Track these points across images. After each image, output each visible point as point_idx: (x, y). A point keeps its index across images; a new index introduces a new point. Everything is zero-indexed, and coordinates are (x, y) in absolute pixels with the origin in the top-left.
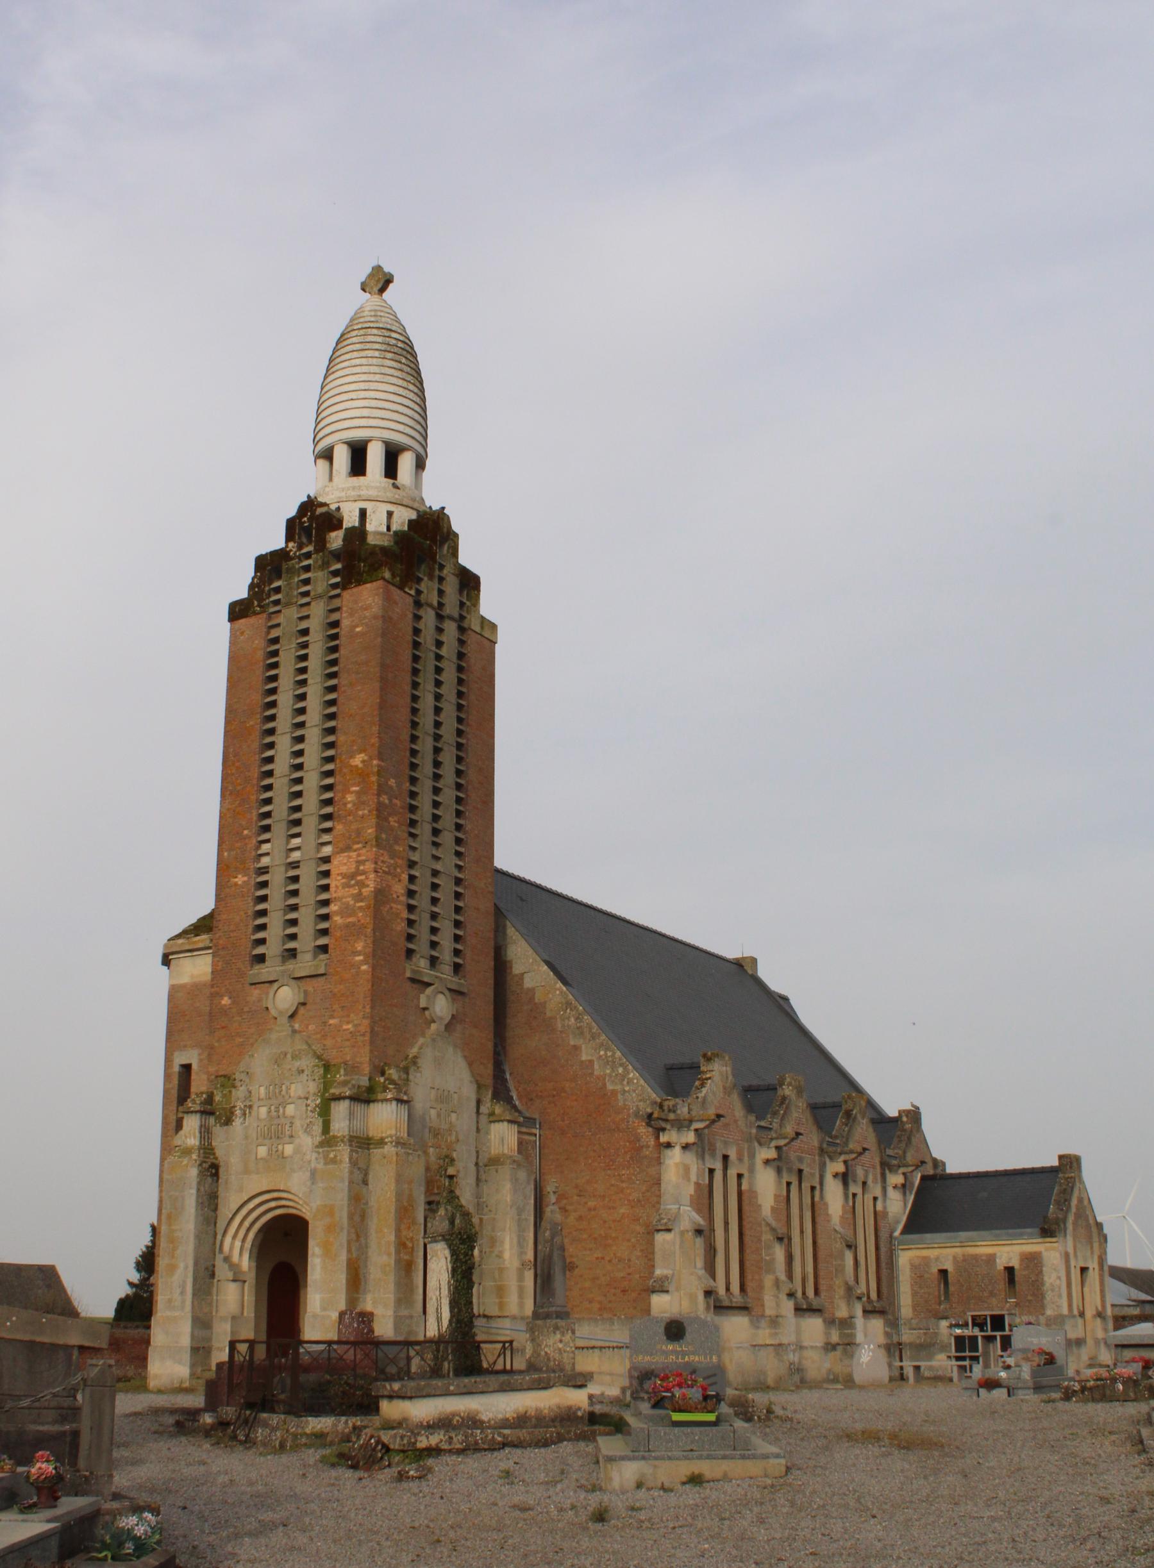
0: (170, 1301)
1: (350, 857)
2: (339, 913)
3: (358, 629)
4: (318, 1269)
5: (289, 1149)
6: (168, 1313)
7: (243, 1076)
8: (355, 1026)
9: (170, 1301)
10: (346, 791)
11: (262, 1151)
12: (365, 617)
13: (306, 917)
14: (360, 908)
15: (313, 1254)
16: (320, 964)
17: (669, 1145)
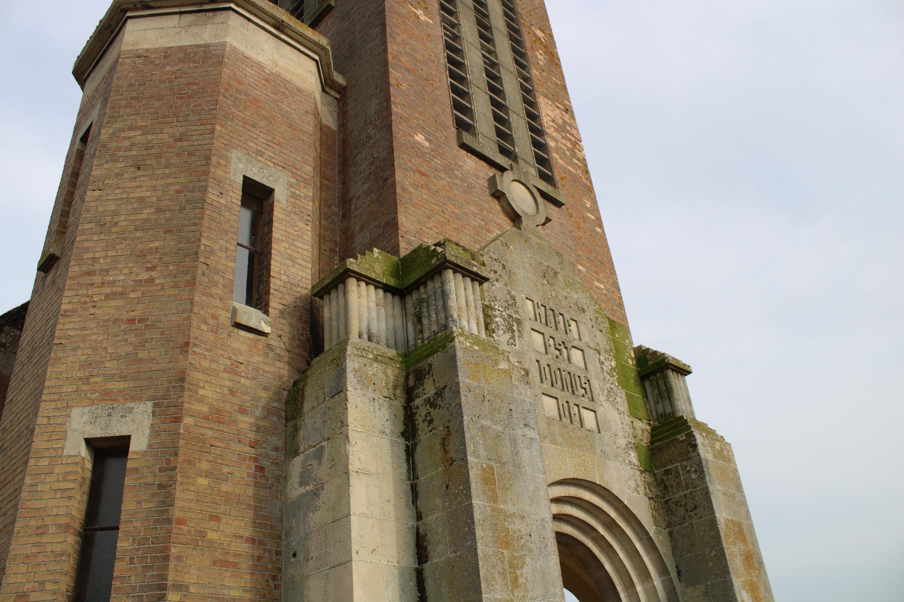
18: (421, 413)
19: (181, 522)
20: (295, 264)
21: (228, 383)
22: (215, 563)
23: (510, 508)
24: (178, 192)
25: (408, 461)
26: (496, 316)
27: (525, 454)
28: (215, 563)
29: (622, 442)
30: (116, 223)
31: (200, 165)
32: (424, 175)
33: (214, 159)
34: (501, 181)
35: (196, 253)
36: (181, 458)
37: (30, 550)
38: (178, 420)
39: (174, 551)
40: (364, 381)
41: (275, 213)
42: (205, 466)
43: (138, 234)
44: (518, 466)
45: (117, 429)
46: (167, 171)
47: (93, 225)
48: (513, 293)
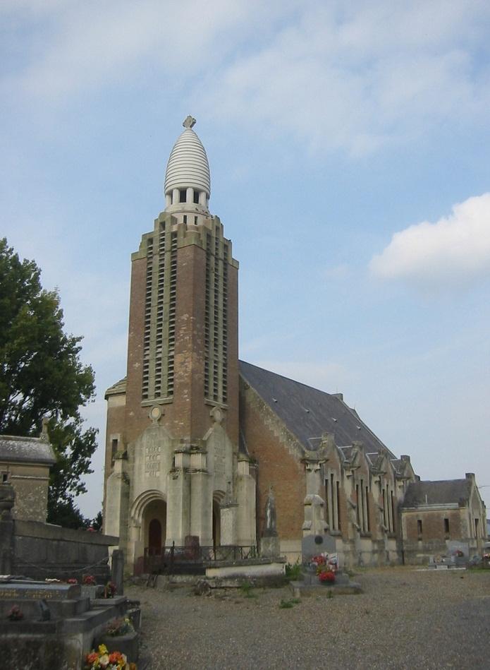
17: (309, 470)
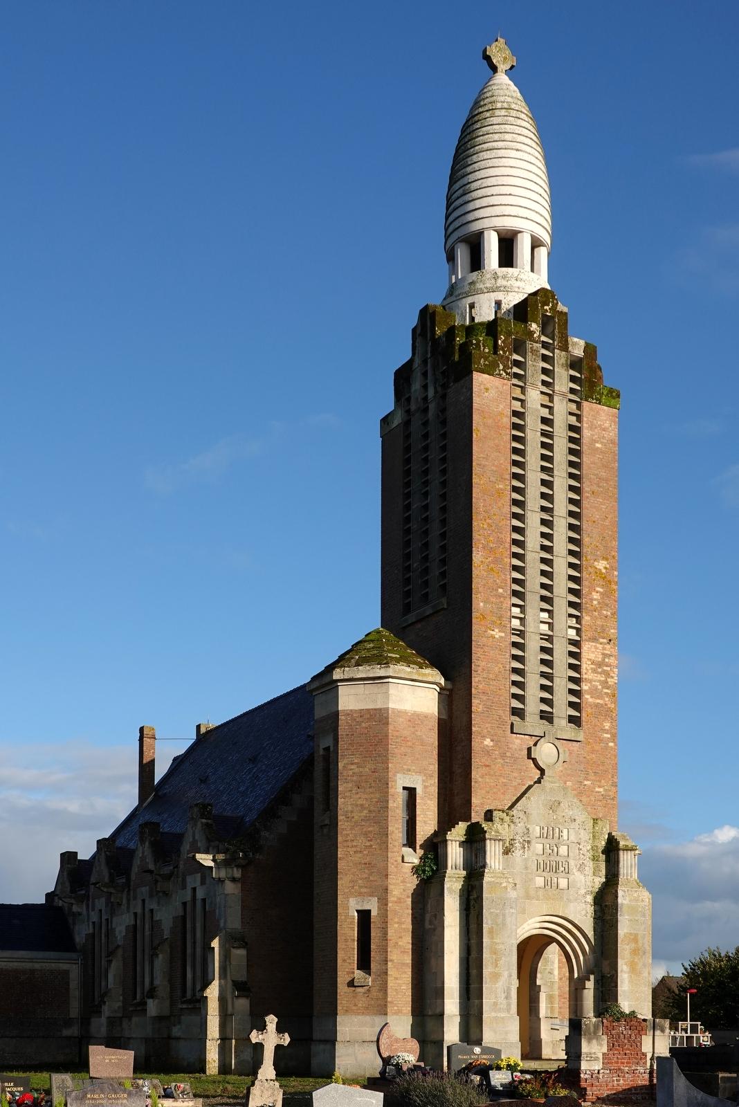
0: (495, 1004)
1: (596, 648)
2: (591, 692)
3: (598, 445)
4: (626, 982)
5: (563, 883)
6: (493, 1014)
7: (521, 815)
8: (605, 790)
9: (495, 1004)
10: (592, 589)
11: (540, 881)
12: (604, 437)
13: (561, 686)
14: (606, 693)
15: (622, 971)
16: (569, 731)
18: (472, 903)
19: (390, 940)
20: (427, 825)
21: (402, 887)
22: (401, 952)
23: (498, 941)
24: (377, 802)
25: (466, 919)
26: (515, 843)
27: (508, 920)
28: (401, 952)
29: (583, 891)
30: (353, 817)
31: (383, 784)
32: (488, 766)
33: (390, 785)
34: (535, 750)
35: (387, 834)
36: (389, 918)
37: (343, 947)
38: (387, 905)
39: (389, 950)
40: (451, 890)
41: (417, 801)
42: (396, 920)
43: (363, 823)
44: (504, 924)
45: (366, 907)
46: (371, 790)
47: (343, 817)
48: (529, 826)
